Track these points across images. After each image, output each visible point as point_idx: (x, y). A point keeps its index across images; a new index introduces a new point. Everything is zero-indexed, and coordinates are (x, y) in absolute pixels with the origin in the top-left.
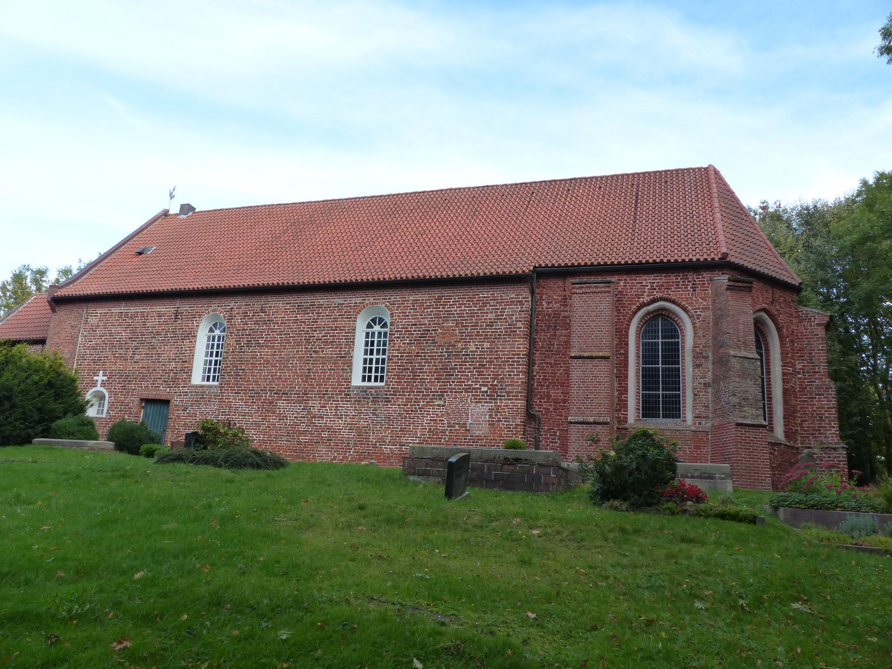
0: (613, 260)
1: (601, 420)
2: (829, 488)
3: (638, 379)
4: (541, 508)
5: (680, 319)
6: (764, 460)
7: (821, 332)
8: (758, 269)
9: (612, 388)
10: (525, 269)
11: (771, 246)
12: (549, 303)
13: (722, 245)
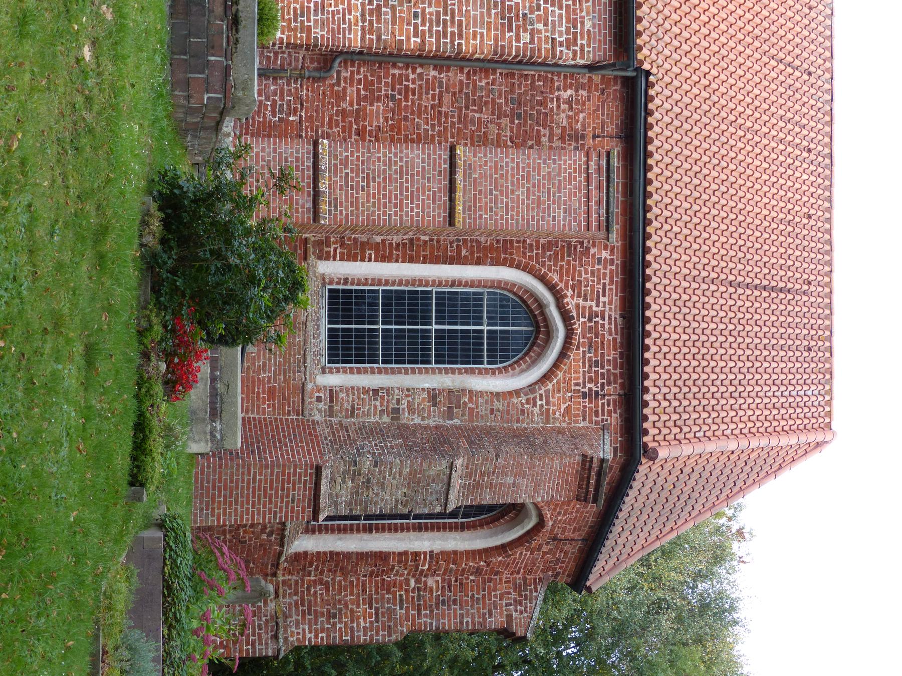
0: (655, 238)
1: (324, 207)
2: (205, 617)
3: (407, 283)
4: (137, 68)
5: (529, 368)
6: (254, 513)
7: (496, 621)
8: (622, 515)
9: (390, 230)
10: (645, 51)
11: (664, 541)
12: (569, 102)
13: (672, 450)
